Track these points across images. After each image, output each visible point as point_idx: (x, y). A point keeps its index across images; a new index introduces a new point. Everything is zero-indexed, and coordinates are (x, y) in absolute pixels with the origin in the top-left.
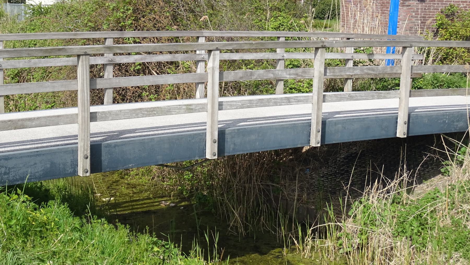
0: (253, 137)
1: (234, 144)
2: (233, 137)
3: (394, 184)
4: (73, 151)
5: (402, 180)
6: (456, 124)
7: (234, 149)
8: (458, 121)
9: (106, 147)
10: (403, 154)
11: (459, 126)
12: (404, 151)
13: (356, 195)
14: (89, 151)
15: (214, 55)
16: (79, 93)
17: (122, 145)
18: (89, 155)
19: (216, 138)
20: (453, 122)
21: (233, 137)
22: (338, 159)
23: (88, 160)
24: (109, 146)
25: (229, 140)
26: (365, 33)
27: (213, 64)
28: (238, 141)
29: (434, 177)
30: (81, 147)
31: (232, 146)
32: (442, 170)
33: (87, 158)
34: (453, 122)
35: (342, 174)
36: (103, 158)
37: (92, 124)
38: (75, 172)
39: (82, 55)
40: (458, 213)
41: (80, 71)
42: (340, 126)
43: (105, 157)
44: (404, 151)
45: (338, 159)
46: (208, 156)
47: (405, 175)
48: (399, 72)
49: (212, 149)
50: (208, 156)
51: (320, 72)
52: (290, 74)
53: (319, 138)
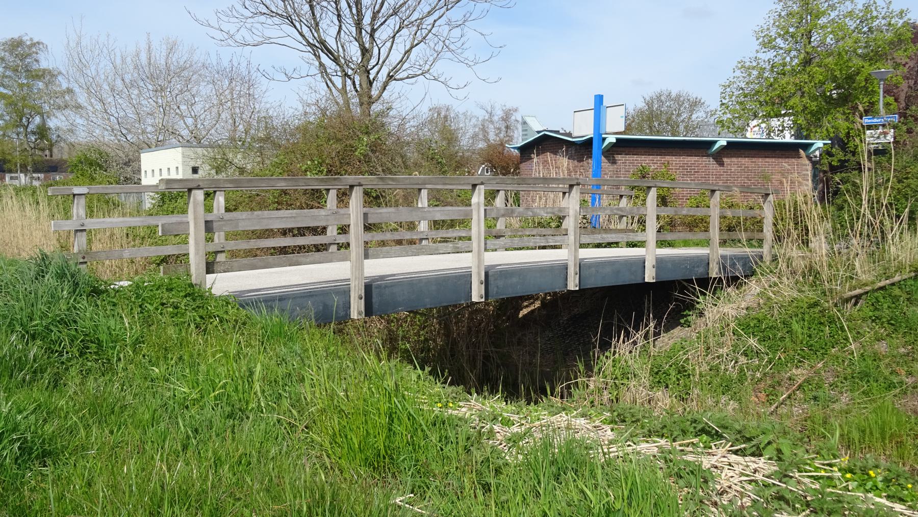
0: (514, 280)
1: (497, 287)
2: (496, 280)
3: (639, 335)
4: (345, 292)
5: (648, 331)
6: (696, 269)
7: (497, 293)
8: (698, 267)
9: (376, 288)
10: (648, 304)
11: (700, 271)
12: (649, 301)
13: (605, 346)
14: (363, 291)
15: (479, 189)
16: (352, 227)
17: (392, 286)
18: (363, 295)
19: (483, 278)
20: (694, 267)
21: (496, 280)
22: (561, 321)
23: (363, 300)
24: (379, 287)
25: (492, 282)
26: (558, 177)
27: (479, 199)
28: (500, 283)
29: (673, 329)
30: (355, 286)
31: (495, 289)
32: (682, 321)
33: (361, 298)
34: (694, 267)
35: (570, 336)
36: (374, 300)
37: (366, 261)
38: (347, 315)
39: (357, 186)
40: (714, 358)
41: (354, 203)
42: (593, 269)
43: (375, 299)
44: (649, 301)
45: (561, 321)
46: (475, 299)
47: (652, 324)
48: (645, 213)
49: (479, 291)
50: (475, 299)
51: (576, 211)
52: (547, 213)
53: (577, 281)
